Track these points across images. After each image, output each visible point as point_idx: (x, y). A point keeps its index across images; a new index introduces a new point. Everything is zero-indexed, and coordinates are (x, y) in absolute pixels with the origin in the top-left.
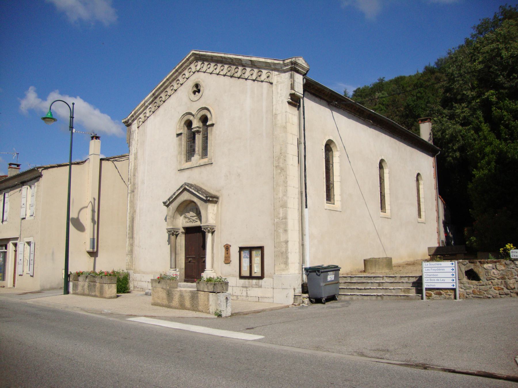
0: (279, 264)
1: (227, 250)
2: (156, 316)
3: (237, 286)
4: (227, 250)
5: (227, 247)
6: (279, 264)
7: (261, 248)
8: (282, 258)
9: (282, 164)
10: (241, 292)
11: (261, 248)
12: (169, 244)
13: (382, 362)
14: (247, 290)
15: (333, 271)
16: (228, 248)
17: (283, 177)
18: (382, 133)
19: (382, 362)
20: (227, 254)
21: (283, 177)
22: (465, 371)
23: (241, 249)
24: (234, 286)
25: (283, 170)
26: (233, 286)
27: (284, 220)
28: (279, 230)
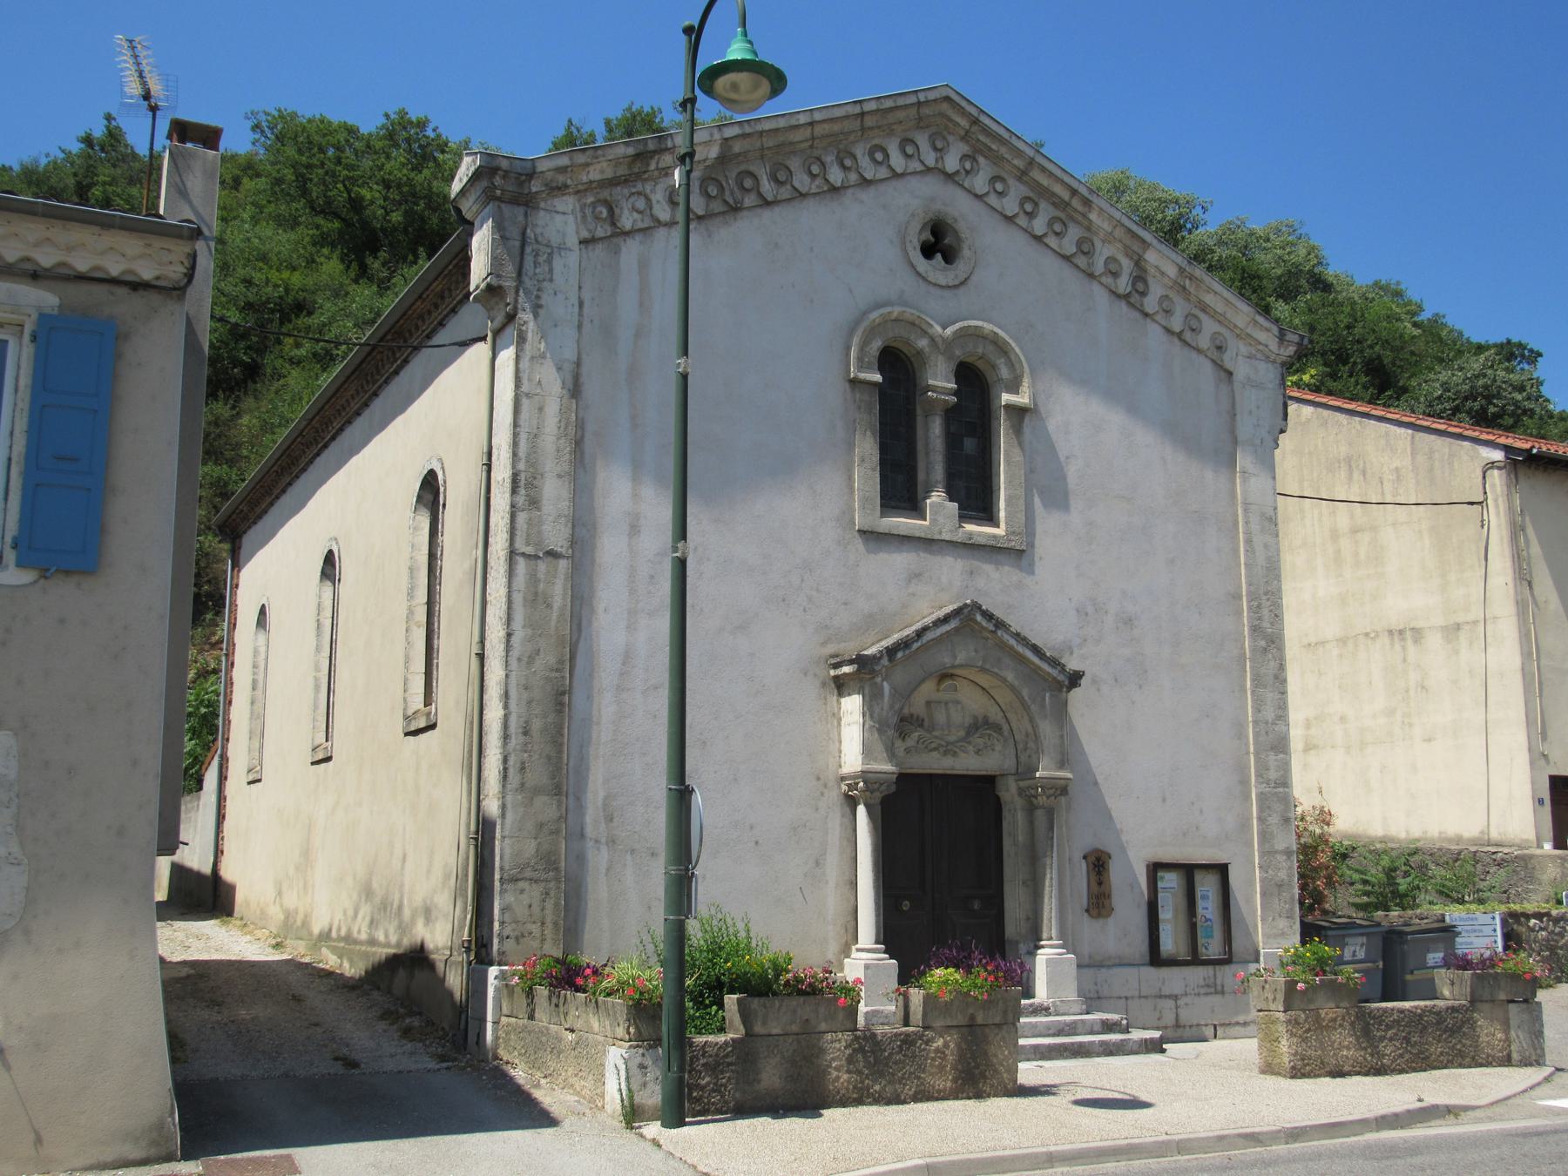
0: (1273, 919)
1: (1099, 873)
2: (1286, 420)
3: (1143, 994)
4: (1099, 873)
5: (1098, 859)
6: (1271, 919)
7: (1222, 870)
8: (1280, 900)
9: (1269, 626)
10: (1157, 1015)
11: (1222, 870)
12: (1163, 1051)
13: (11, 447)
14: (1177, 1007)
15: (1362, 935)
16: (1102, 866)
17: (1272, 663)
18: (539, 1130)
19: (11, 447)
20: (1100, 884)
21: (1272, 663)
22: (485, 729)
23: (1155, 868)
24: (1133, 997)
25: (1273, 642)
26: (1126, 998)
27: (1281, 790)
28: (1270, 816)
